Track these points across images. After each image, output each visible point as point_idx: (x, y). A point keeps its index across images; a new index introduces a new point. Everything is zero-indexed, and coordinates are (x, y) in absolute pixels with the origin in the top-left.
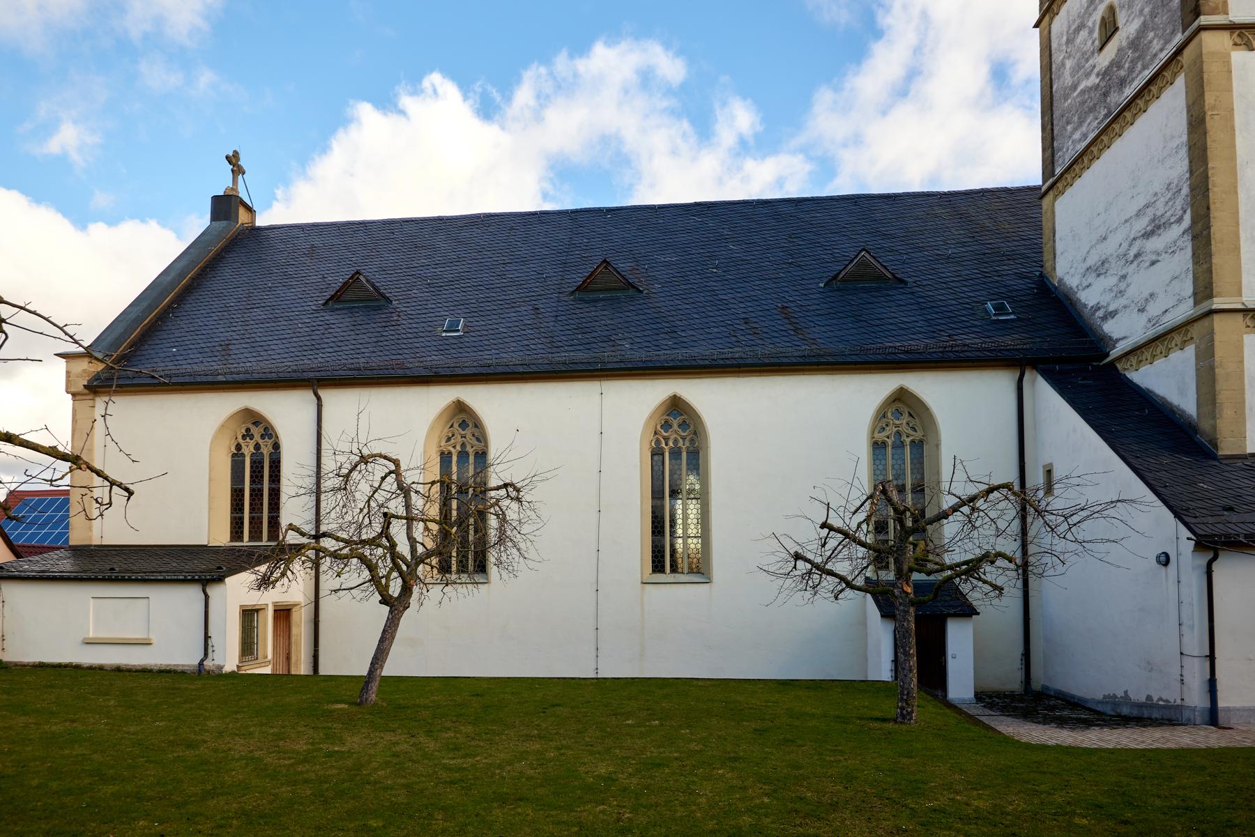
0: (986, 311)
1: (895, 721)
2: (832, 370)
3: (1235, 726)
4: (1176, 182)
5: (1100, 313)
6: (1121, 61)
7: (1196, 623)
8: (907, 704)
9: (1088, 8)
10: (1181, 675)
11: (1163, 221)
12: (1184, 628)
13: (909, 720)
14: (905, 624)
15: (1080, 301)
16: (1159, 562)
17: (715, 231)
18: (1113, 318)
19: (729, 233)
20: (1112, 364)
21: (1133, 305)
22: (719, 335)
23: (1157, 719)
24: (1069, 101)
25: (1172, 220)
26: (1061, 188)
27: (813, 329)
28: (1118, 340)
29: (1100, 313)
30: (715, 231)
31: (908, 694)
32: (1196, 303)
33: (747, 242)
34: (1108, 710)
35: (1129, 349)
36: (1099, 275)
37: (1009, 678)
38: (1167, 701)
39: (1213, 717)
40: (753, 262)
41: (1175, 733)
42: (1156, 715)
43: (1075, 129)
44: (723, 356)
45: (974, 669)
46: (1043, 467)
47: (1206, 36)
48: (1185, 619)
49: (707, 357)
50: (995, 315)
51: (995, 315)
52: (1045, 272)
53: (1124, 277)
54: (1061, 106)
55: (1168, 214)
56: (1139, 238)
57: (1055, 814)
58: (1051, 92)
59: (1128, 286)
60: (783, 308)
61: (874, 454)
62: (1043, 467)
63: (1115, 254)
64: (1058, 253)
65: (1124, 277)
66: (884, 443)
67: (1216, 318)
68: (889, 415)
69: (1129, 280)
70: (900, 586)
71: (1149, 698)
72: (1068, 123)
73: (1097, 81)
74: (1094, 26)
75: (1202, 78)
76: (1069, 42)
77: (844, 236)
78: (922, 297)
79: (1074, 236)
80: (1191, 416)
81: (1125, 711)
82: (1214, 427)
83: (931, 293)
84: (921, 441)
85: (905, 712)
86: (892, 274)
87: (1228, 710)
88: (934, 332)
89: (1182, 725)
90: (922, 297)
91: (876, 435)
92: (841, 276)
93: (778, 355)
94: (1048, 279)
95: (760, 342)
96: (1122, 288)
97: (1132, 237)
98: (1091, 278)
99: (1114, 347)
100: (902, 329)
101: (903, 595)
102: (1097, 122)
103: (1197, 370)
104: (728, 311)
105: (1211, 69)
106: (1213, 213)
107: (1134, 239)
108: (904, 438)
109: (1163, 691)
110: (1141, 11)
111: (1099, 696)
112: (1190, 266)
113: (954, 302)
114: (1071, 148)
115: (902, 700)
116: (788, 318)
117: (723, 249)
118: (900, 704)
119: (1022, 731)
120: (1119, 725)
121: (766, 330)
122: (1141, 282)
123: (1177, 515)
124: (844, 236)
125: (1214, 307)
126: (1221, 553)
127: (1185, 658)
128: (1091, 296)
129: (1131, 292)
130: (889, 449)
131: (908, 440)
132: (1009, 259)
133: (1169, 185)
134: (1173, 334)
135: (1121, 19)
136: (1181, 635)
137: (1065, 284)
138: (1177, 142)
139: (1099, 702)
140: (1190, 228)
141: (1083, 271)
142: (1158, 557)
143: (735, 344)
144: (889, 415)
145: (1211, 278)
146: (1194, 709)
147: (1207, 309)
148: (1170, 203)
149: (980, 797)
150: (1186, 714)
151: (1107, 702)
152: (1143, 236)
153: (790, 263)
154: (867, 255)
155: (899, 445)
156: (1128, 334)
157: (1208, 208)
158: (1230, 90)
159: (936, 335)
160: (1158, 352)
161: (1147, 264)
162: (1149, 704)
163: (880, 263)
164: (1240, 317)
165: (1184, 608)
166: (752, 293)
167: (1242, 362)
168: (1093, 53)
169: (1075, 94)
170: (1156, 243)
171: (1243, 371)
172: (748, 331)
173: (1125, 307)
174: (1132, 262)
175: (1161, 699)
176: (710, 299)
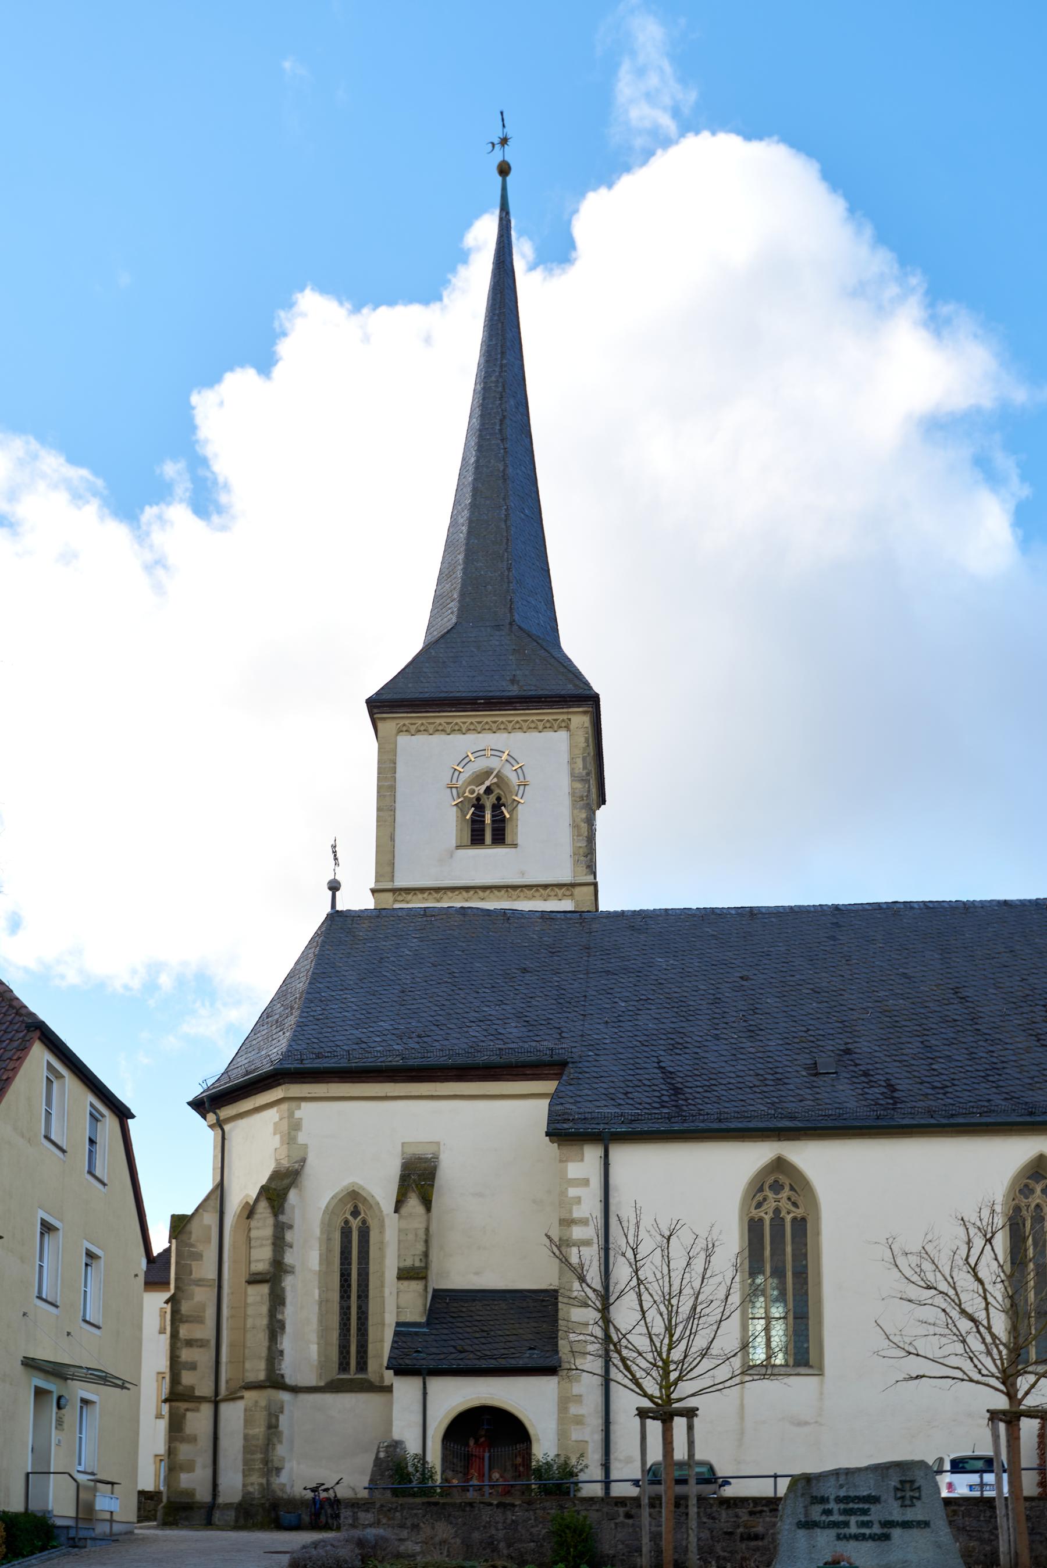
84: (804, 1219)
131: (788, 1218)
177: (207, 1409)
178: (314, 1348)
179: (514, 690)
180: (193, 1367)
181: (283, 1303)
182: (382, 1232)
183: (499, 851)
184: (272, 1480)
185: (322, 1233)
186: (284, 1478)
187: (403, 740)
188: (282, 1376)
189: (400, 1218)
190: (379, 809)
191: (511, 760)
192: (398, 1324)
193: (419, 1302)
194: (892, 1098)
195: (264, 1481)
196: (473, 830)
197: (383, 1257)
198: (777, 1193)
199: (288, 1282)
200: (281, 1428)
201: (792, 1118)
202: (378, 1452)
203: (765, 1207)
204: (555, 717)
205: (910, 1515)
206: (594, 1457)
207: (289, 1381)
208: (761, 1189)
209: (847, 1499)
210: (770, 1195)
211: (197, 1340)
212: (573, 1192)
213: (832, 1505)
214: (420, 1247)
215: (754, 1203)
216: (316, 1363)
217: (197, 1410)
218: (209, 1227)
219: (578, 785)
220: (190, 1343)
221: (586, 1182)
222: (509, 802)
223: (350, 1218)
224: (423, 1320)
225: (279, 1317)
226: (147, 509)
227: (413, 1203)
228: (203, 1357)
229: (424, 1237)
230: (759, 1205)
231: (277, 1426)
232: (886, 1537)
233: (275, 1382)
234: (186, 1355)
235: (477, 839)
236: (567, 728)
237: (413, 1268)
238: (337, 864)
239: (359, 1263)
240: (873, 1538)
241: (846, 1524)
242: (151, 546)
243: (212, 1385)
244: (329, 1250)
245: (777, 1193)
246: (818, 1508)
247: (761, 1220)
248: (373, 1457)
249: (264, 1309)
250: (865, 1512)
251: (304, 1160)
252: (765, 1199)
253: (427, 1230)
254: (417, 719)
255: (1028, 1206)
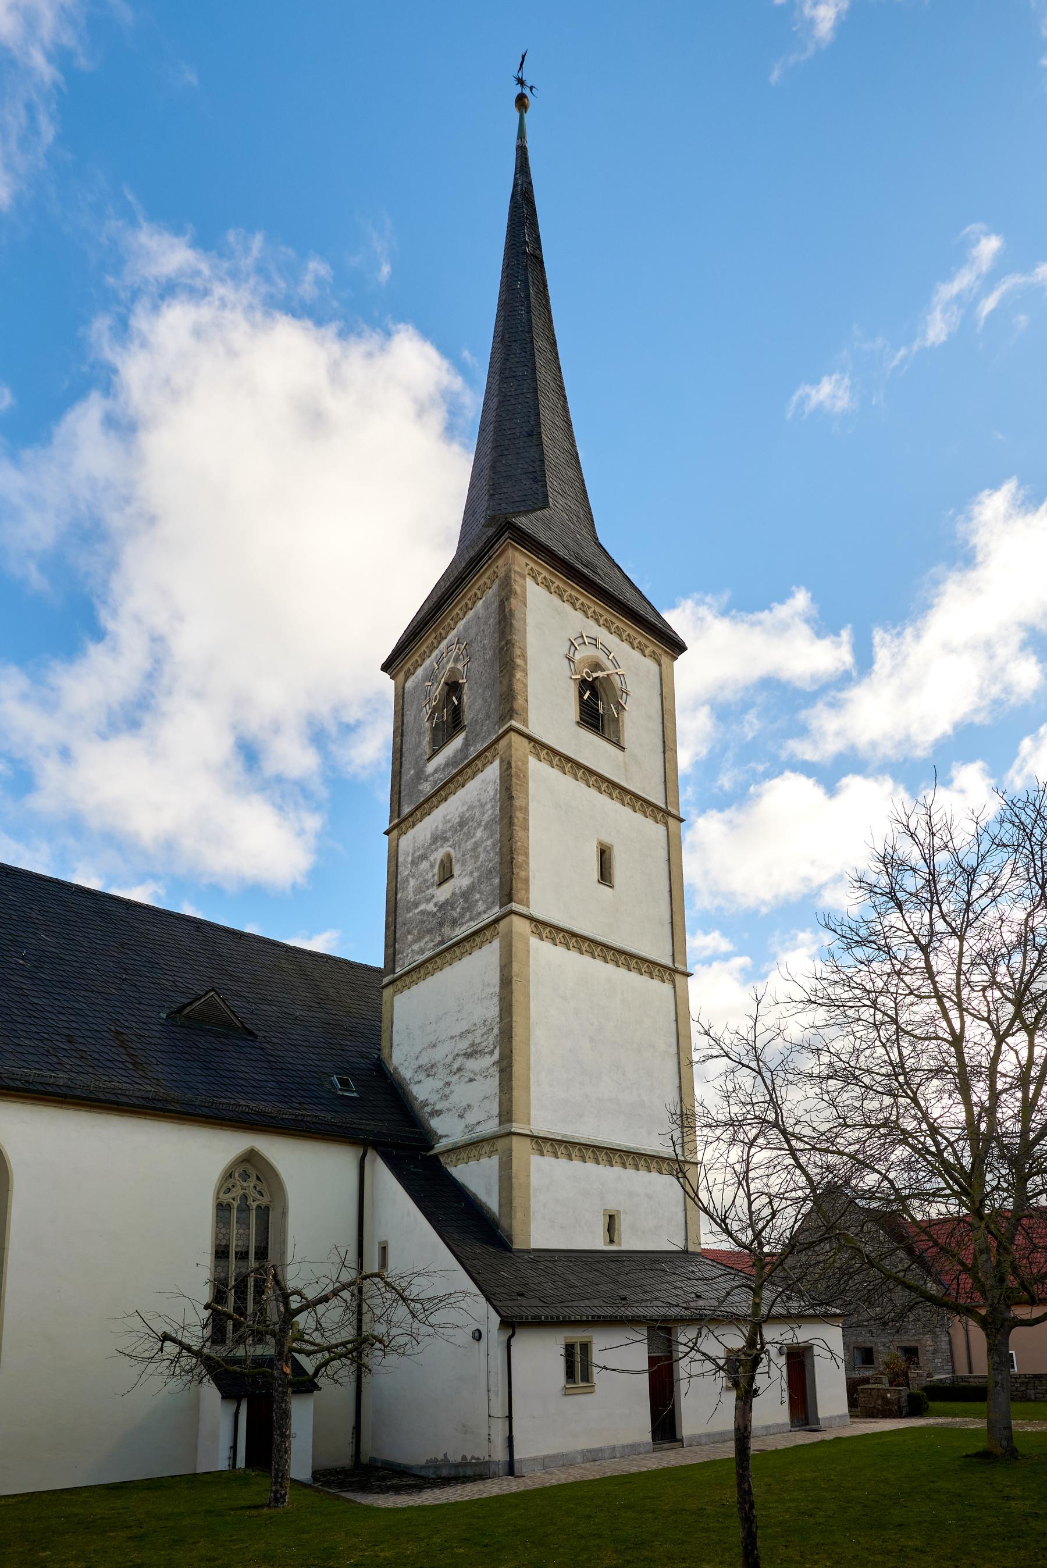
0: (332, 1083)
1: (269, 1506)
2: (179, 1119)
3: (525, 1474)
4: (490, 1020)
5: (428, 1109)
6: (454, 904)
7: (500, 1389)
8: (281, 1486)
9: (431, 844)
10: (489, 1435)
11: (479, 1049)
12: (491, 1394)
13: (283, 1502)
14: (283, 1405)
15: (412, 1093)
16: (474, 1337)
17: (18, 908)
18: (438, 1116)
19: (40, 917)
20: (436, 1157)
21: (454, 1110)
22: (33, 1051)
23: (470, 1476)
24: (411, 914)
25: (486, 1051)
26: (400, 987)
27: (156, 1067)
28: (441, 1137)
29: (428, 1109)
30: (18, 908)
31: (283, 1476)
32: (501, 1123)
33: (66, 936)
34: (430, 1473)
35: (450, 1147)
36: (428, 1076)
37: (341, 1455)
38: (478, 1459)
39: (511, 1468)
40: (75, 964)
41: (487, 1485)
42: (470, 1472)
43: (415, 941)
44: (42, 1080)
45: (313, 1446)
46: (379, 1243)
47: (515, 918)
48: (492, 1388)
49: (18, 1077)
50: (340, 1090)
51: (340, 1090)
52: (382, 1057)
53: (448, 1084)
54: (404, 916)
55: (484, 1044)
56: (462, 1055)
57: (440, 1550)
58: (396, 898)
59: (451, 1092)
60: (118, 1033)
61: (217, 1216)
62: (379, 1243)
63: (442, 1062)
64: (395, 1043)
65: (448, 1084)
66: (229, 1205)
67: (514, 1138)
68: (237, 1175)
69: (452, 1087)
70: (280, 1367)
71: (464, 1457)
72: (409, 933)
73: (435, 910)
74: (435, 863)
75: (511, 950)
76: (413, 863)
77: (187, 964)
78: (272, 1056)
79: (409, 1034)
80: (494, 1214)
81: (445, 1472)
82: (511, 1225)
83: (279, 1053)
84: (267, 1208)
85: (279, 1495)
86: (242, 1023)
87: (521, 1461)
88: (285, 1096)
89: (490, 1478)
90: (272, 1056)
91: (221, 1195)
92: (186, 1012)
93: (116, 1091)
94: (384, 1063)
95: (90, 1070)
96: (447, 1093)
97: (456, 1053)
98: (421, 1076)
99: (438, 1142)
100: (254, 1087)
101: (282, 1376)
102: (433, 944)
103: (500, 1177)
104: (44, 1021)
105: (517, 946)
106: (515, 1057)
107: (458, 1055)
108: (250, 1202)
109: (476, 1451)
110: (472, 873)
111: (422, 1461)
112: (498, 1091)
113: (302, 1068)
114: (410, 955)
115: (276, 1483)
116: (124, 1048)
117: (31, 935)
118: (274, 1488)
119: (775, 1372)
120: (442, 1485)
121: (97, 1056)
122: (462, 1093)
123: (488, 1299)
124: (187, 964)
125: (513, 1130)
126: (517, 1330)
127: (491, 1419)
128: (422, 1091)
129: (454, 1098)
130: (235, 1214)
131: (254, 1205)
132: (351, 1035)
133: (485, 1021)
134: (484, 1143)
135: (457, 870)
136: (489, 1400)
137: (399, 1073)
138: (491, 990)
139: (422, 1467)
140: (499, 1062)
141: (416, 1066)
142: (473, 1333)
143: (57, 1066)
144: (237, 1175)
145: (512, 1106)
146: (497, 1463)
147: (507, 1131)
148: (485, 1036)
149: (382, 1550)
150: (493, 1468)
151: (429, 1467)
152: (464, 1054)
153: (124, 980)
154: (216, 996)
155: (244, 1209)
156: (450, 1134)
157: (511, 1052)
158: (528, 966)
159: (287, 1100)
160: (472, 1155)
161: (467, 1079)
162: (464, 1464)
163: (228, 1006)
164: (528, 1140)
165: (492, 1374)
166: (76, 1005)
167: (529, 1176)
168: (433, 884)
169: (416, 911)
170: (472, 1064)
171: (529, 1183)
172: (73, 1053)
173: (448, 1110)
174: (455, 1074)
175: (473, 1458)
176: (17, 998)
226: (716, 934)
242: (1023, 1456)
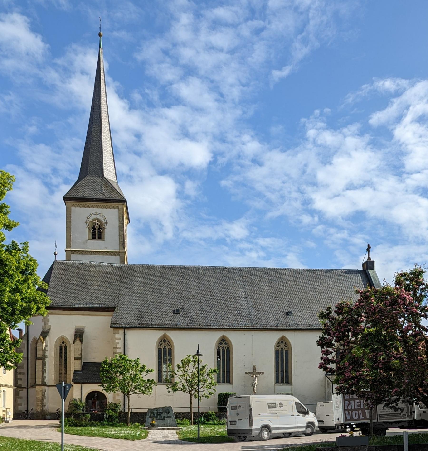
177: (25, 390)
178: (53, 376)
179: (103, 197)
180: (21, 379)
181: (45, 365)
182: (70, 348)
183: (100, 242)
184: (43, 408)
185: (55, 347)
186: (46, 407)
187: (73, 208)
188: (46, 383)
189: (75, 345)
190: (67, 228)
191: (103, 216)
192: (75, 371)
193: (80, 366)
194: (191, 320)
195: (41, 408)
196: (92, 234)
197: (70, 354)
198: (165, 342)
199: (47, 360)
200: (45, 395)
201: (168, 325)
202: (70, 402)
203: (162, 346)
204: (115, 205)
205: (168, 415)
206: (122, 403)
207: (47, 384)
208: (161, 341)
209: (157, 413)
210: (163, 342)
211: (22, 373)
212: (117, 341)
213: (155, 414)
214: (80, 352)
215: (160, 345)
216: (54, 380)
217: (22, 390)
218: (25, 344)
219: (121, 225)
220: (20, 373)
221: (120, 339)
222: (103, 228)
223: (62, 344)
224: (81, 370)
225: (45, 368)
227: (78, 341)
228: (24, 377)
229: (80, 350)
230: (161, 345)
231: (44, 395)
232: (164, 419)
233: (44, 384)
234: (19, 376)
235: (94, 238)
236: (118, 209)
237: (78, 357)
238: (56, 247)
239: (64, 355)
240: (162, 419)
241: (157, 417)
243: (26, 384)
244: (57, 352)
245: (165, 342)
246: (152, 414)
247: (161, 349)
248: (69, 403)
249: (41, 367)
250: (161, 415)
251: (50, 329)
252: (162, 344)
253: (81, 348)
254: (77, 203)
255: (221, 347)
